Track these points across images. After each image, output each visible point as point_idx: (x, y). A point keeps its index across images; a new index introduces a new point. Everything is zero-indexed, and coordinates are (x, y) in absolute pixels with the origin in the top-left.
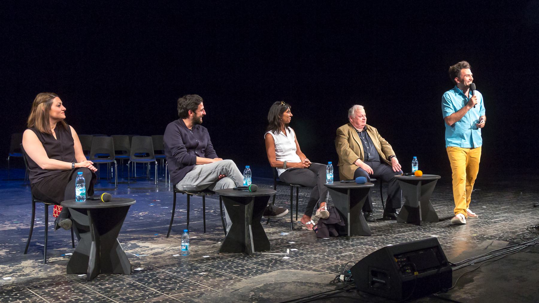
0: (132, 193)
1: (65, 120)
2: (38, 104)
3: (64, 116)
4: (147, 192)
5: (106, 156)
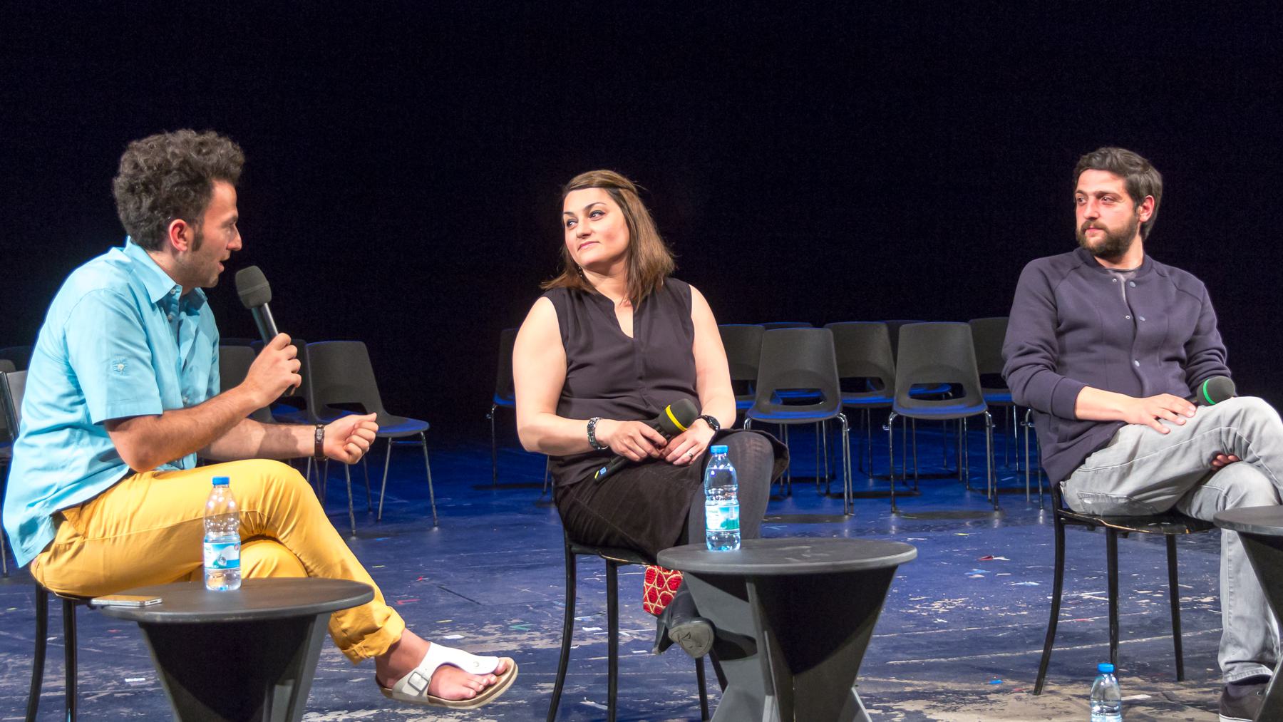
0: (906, 529)
5: (812, 399)
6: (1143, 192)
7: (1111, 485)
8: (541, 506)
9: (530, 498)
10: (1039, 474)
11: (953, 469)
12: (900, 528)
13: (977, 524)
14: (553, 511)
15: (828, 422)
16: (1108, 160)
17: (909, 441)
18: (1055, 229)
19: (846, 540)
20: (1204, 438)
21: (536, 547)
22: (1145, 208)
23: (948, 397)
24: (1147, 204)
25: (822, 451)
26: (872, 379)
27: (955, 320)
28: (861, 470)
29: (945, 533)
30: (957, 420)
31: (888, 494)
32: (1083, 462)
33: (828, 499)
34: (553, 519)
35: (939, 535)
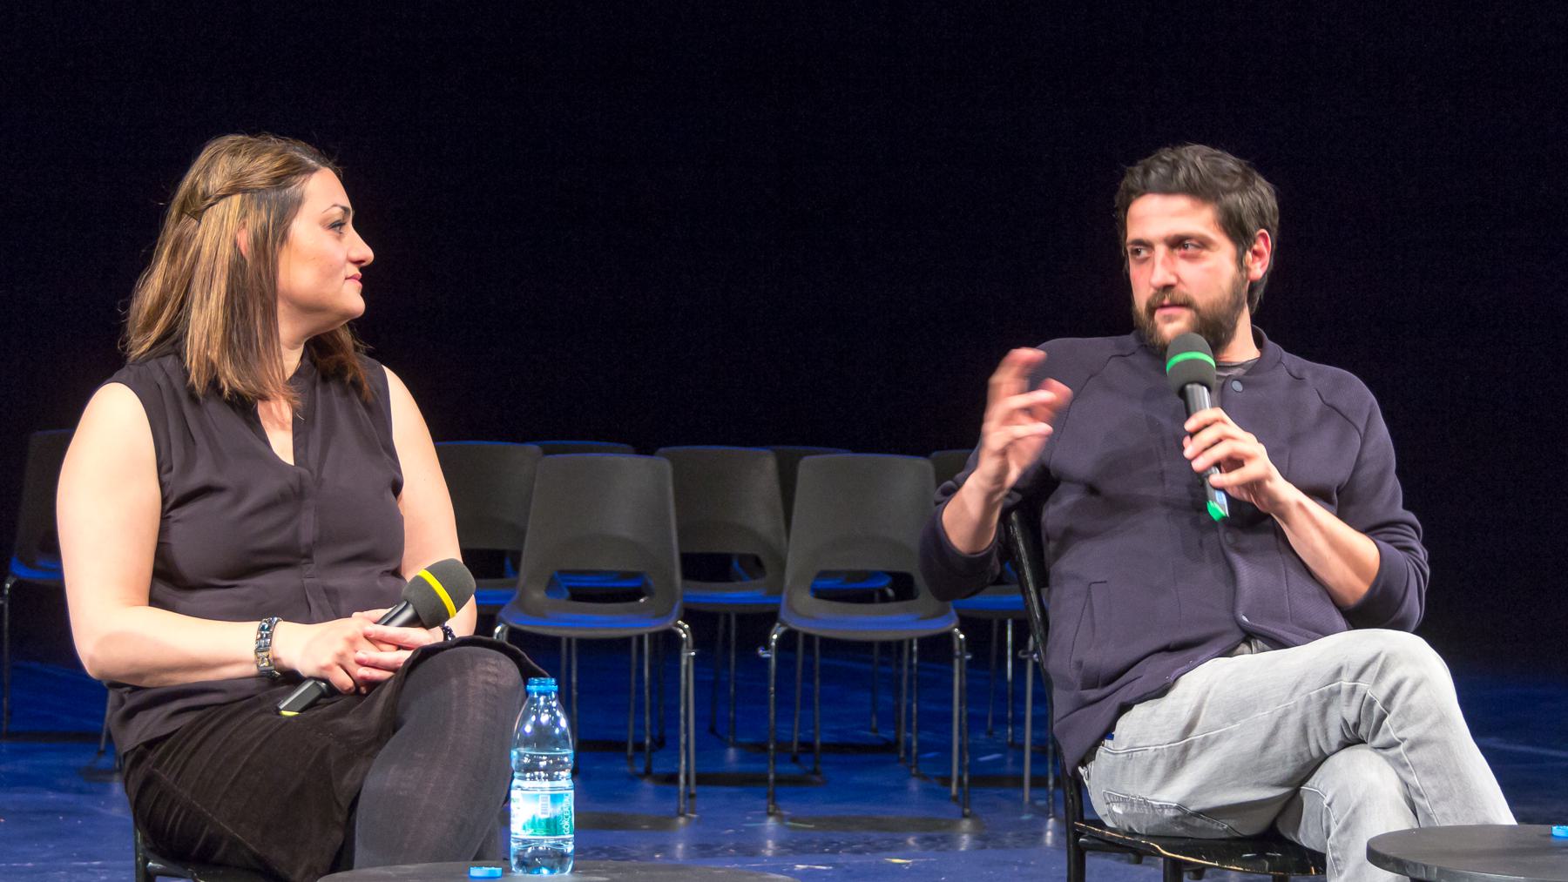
0: (794, 847)
1: (358, 325)
2: (196, 208)
3: (353, 300)
4: (896, 847)
5: (624, 591)
6: (1251, 224)
7: (1153, 782)
8: (95, 779)
9: (72, 762)
10: (1047, 750)
11: (889, 735)
12: (781, 844)
13: (929, 841)
14: (117, 788)
15: (654, 637)
16: (1182, 174)
17: (808, 677)
18: (1086, 295)
19: (678, 867)
20: (1308, 701)
21: (81, 857)
22: (1256, 254)
23: (885, 599)
24: (1260, 245)
25: (640, 691)
26: (743, 558)
27: (903, 451)
28: (713, 731)
29: (868, 859)
30: (900, 643)
31: (765, 780)
32: (1108, 733)
33: (647, 784)
34: (116, 805)
35: (856, 860)
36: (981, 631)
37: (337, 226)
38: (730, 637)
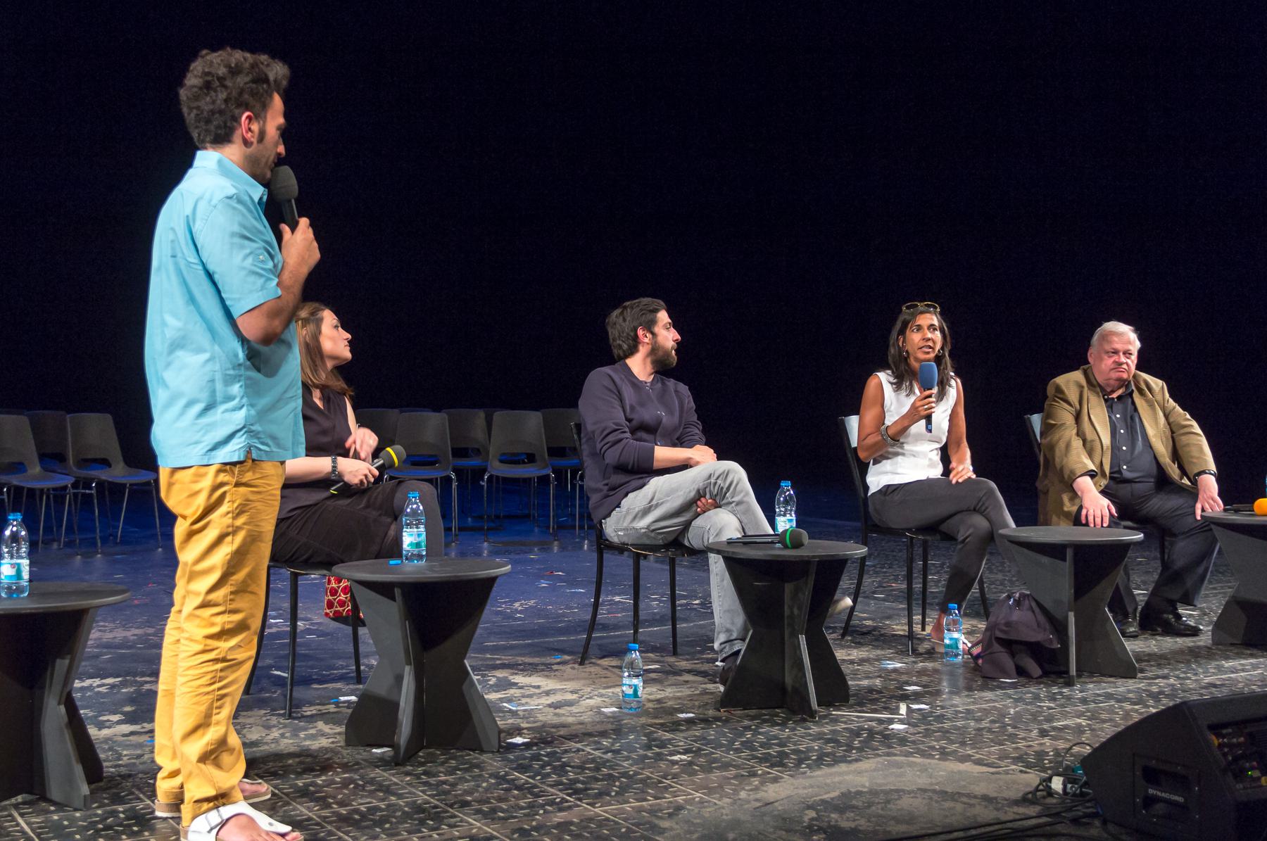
4: (531, 552)
10: (587, 516)
26: (473, 449)
29: (521, 556)
30: (530, 479)
36: (559, 473)
37: (336, 327)
38: (469, 478)
